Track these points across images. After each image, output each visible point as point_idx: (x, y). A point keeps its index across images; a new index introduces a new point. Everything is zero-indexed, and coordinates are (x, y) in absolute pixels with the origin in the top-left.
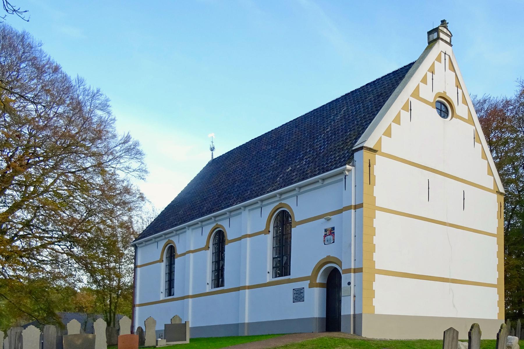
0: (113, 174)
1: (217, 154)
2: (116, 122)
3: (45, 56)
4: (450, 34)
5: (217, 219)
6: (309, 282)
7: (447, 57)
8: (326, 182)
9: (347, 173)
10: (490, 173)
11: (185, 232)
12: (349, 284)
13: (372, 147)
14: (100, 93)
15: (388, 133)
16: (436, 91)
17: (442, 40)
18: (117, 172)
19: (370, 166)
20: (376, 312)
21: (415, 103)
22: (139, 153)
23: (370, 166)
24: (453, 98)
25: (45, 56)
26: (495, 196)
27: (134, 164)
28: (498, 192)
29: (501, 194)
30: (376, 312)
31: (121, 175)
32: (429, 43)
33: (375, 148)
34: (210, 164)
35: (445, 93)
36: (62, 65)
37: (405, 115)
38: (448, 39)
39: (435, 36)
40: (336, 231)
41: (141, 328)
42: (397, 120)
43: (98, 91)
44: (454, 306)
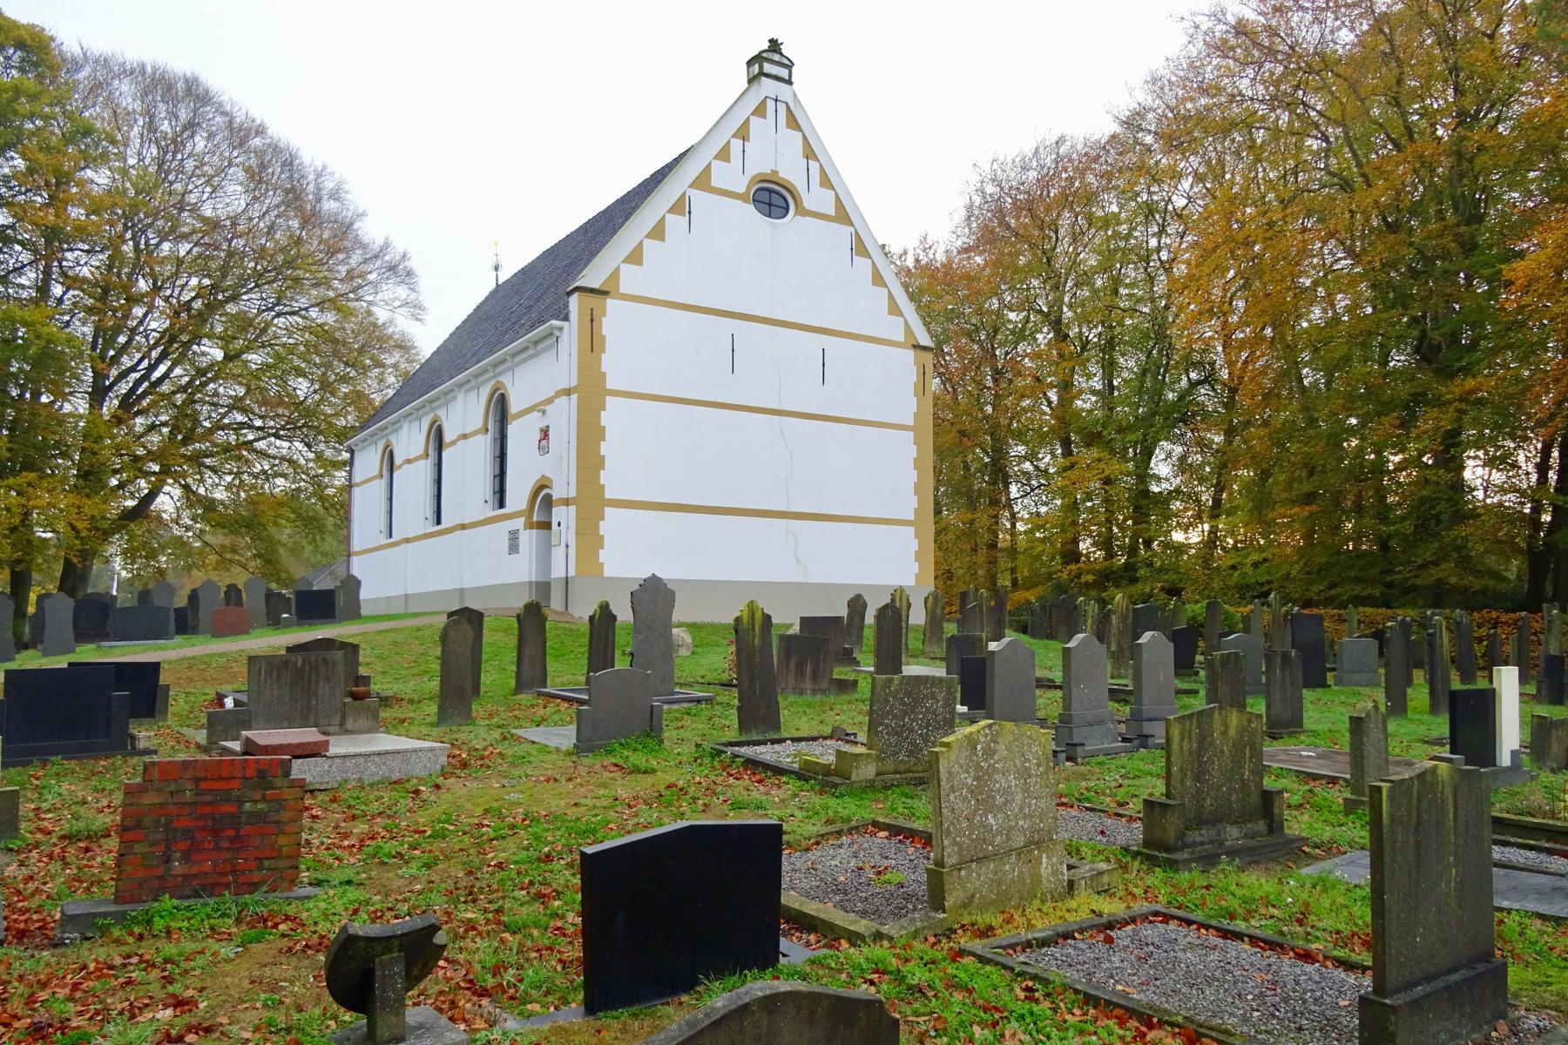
0: (369, 313)
1: (505, 276)
2: (367, 219)
3: (240, 110)
4: (788, 63)
5: (434, 405)
6: (523, 519)
7: (782, 108)
8: (539, 347)
9: (557, 333)
10: (894, 309)
11: (401, 427)
12: (559, 524)
13: (596, 286)
14: (329, 170)
15: (636, 257)
16: (752, 171)
17: (768, 76)
18: (374, 309)
19: (592, 320)
20: (606, 574)
21: (699, 198)
22: (409, 274)
23: (592, 320)
24: (798, 182)
25: (240, 110)
26: (910, 354)
27: (402, 292)
28: (917, 347)
29: (925, 349)
30: (606, 574)
31: (381, 315)
32: (750, 81)
33: (603, 289)
34: (493, 294)
35: (775, 172)
36: (268, 123)
37: (675, 223)
38: (784, 73)
39: (756, 69)
40: (551, 433)
41: (865, 606)
42: (658, 232)
43: (324, 168)
44: (799, 561)
